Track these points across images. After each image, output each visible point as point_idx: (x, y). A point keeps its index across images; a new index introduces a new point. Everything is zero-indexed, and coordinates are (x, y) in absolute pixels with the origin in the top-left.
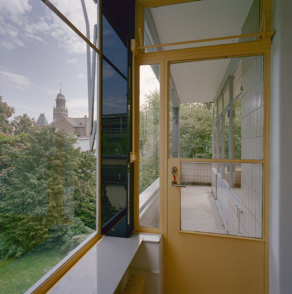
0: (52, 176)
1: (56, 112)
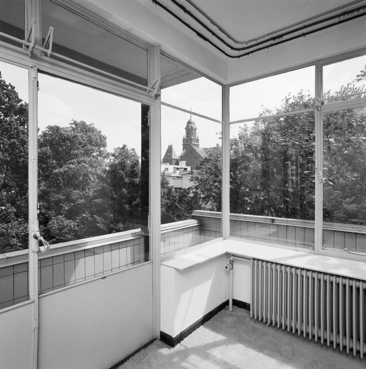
0: (9, 103)
1: (186, 142)
